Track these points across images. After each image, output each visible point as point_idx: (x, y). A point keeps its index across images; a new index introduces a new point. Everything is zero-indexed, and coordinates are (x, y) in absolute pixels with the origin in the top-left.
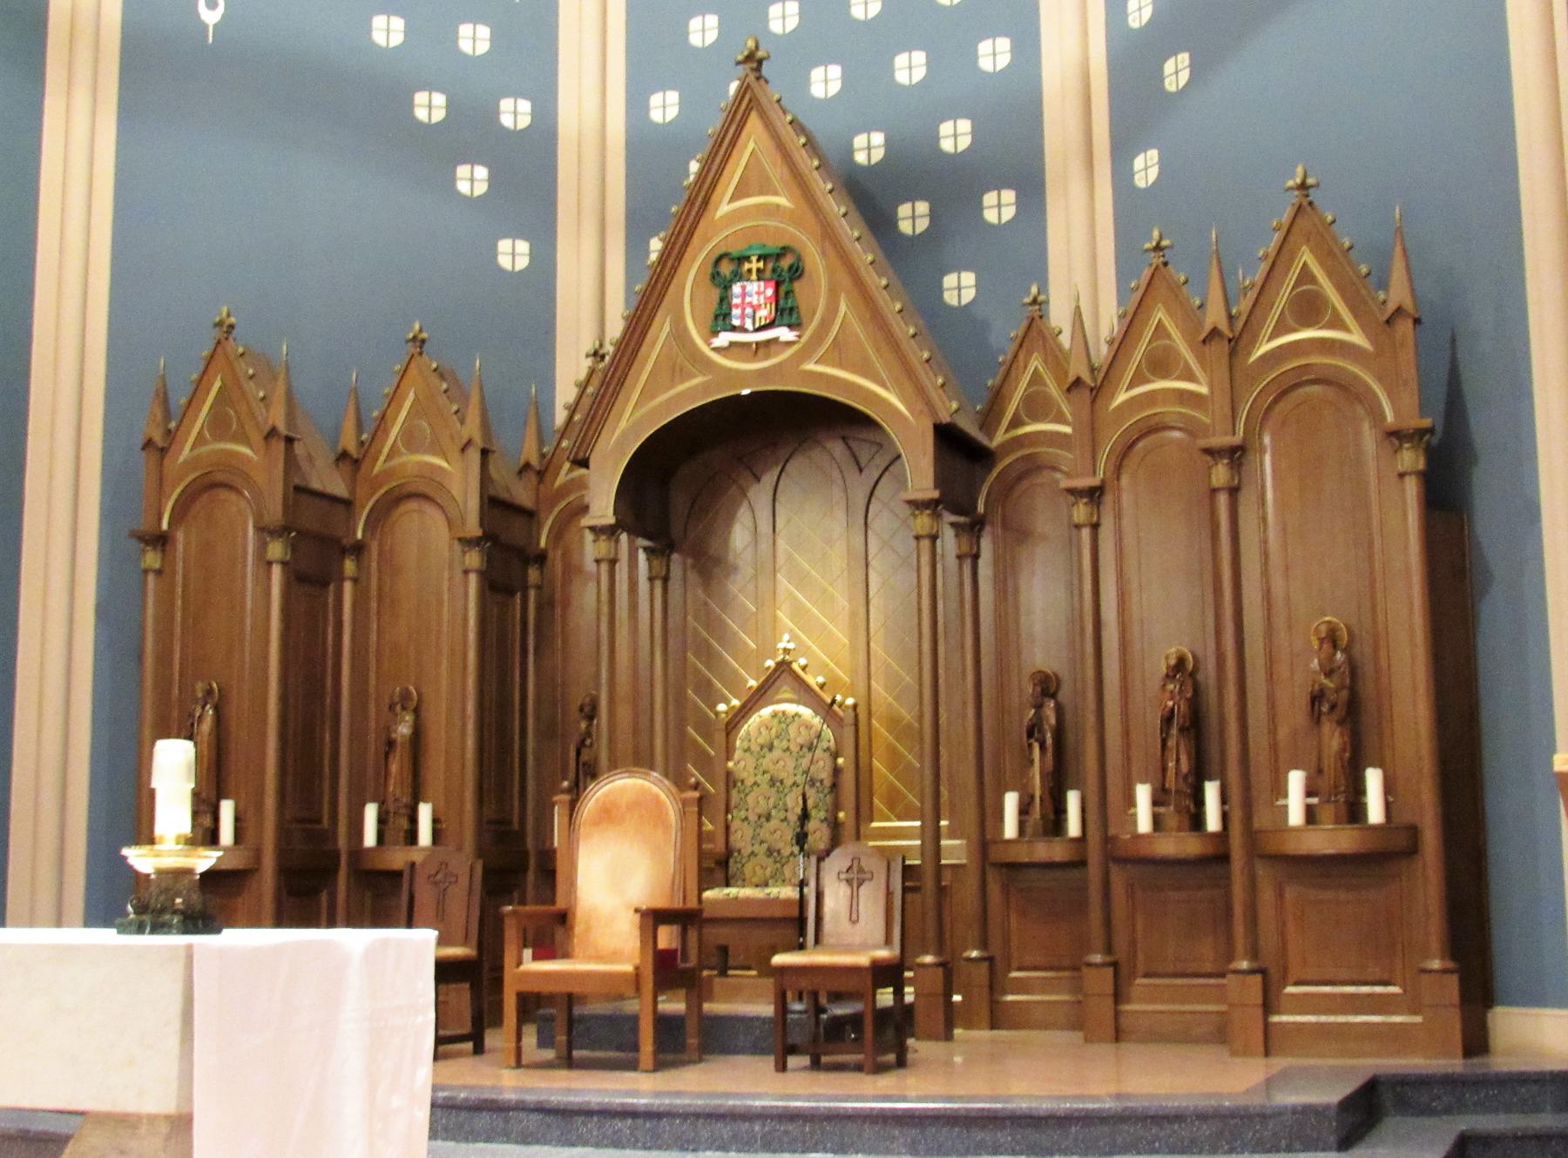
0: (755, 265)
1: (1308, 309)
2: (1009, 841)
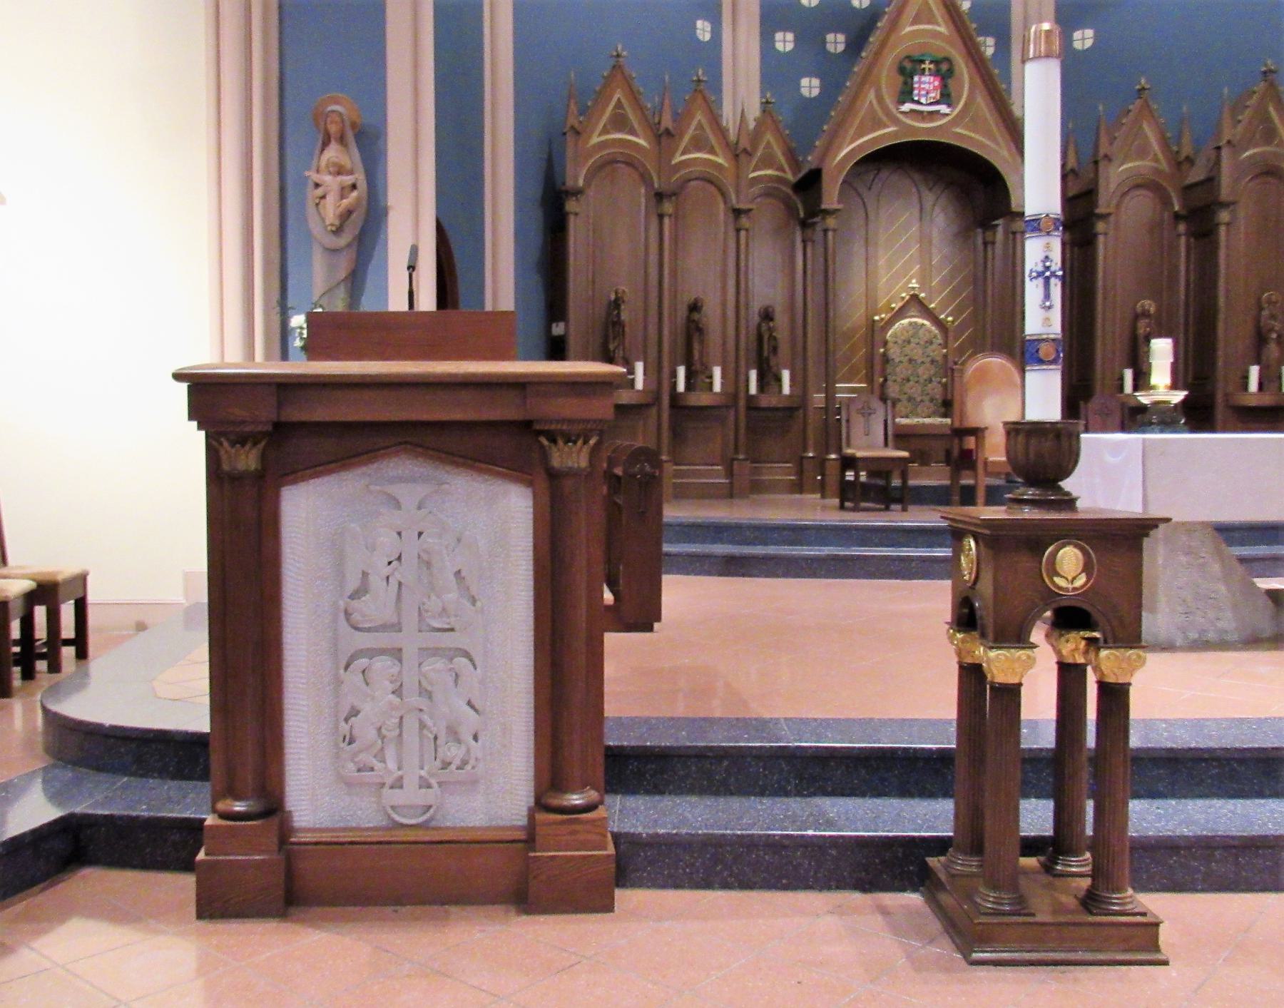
0: (927, 66)
1: (619, 122)
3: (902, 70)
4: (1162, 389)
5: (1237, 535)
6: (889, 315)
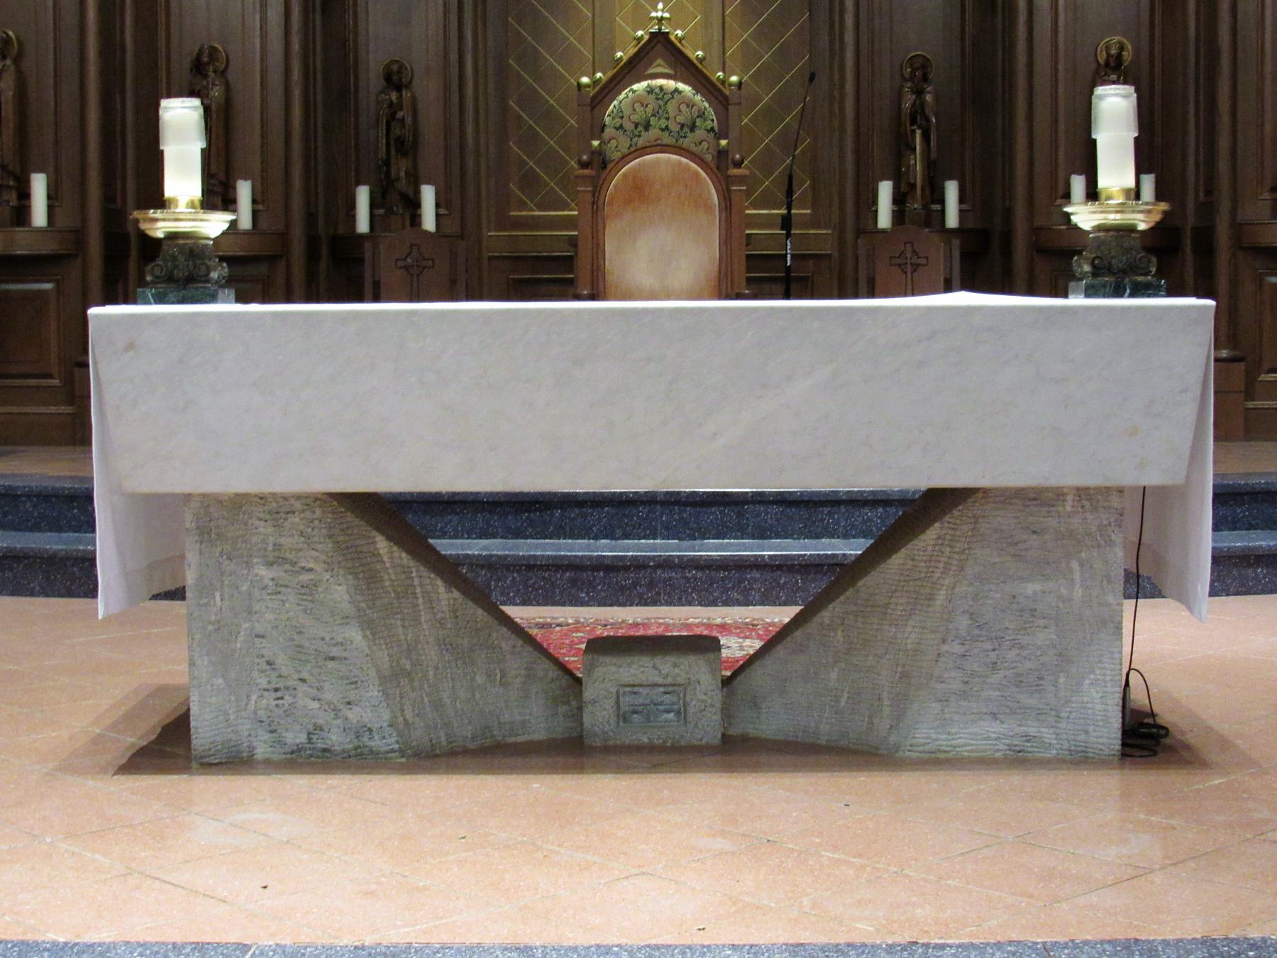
2: (883, 231)
4: (182, 207)
5: (594, 515)
6: (610, 74)
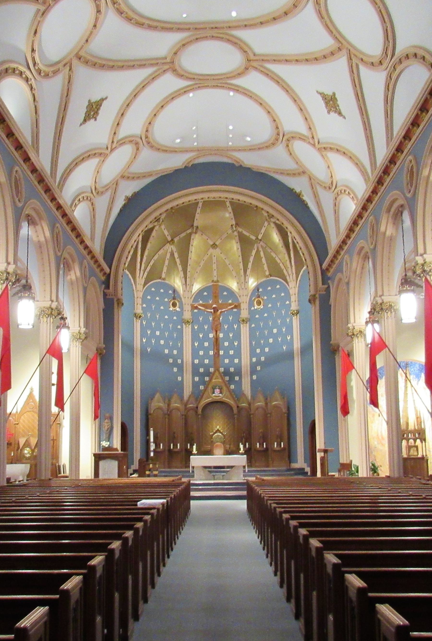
0: (217, 387)
3: (213, 388)
